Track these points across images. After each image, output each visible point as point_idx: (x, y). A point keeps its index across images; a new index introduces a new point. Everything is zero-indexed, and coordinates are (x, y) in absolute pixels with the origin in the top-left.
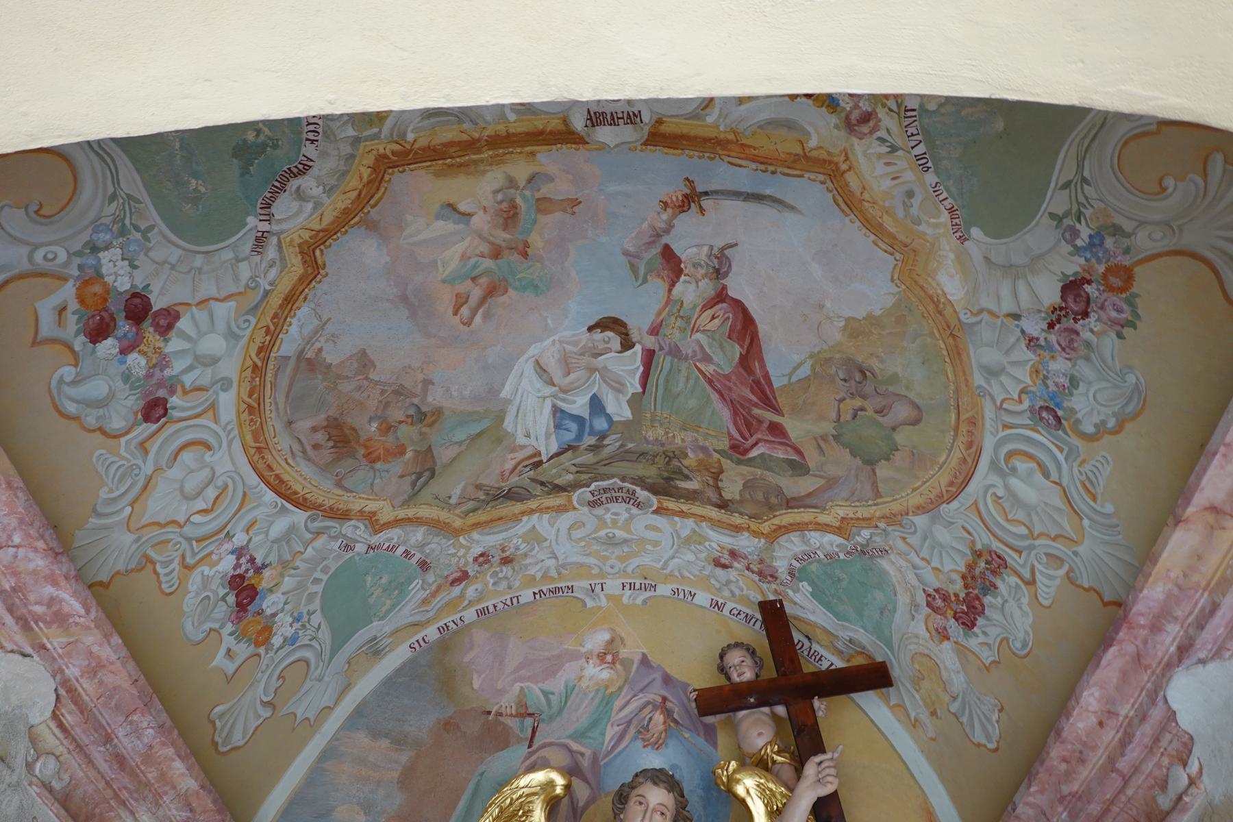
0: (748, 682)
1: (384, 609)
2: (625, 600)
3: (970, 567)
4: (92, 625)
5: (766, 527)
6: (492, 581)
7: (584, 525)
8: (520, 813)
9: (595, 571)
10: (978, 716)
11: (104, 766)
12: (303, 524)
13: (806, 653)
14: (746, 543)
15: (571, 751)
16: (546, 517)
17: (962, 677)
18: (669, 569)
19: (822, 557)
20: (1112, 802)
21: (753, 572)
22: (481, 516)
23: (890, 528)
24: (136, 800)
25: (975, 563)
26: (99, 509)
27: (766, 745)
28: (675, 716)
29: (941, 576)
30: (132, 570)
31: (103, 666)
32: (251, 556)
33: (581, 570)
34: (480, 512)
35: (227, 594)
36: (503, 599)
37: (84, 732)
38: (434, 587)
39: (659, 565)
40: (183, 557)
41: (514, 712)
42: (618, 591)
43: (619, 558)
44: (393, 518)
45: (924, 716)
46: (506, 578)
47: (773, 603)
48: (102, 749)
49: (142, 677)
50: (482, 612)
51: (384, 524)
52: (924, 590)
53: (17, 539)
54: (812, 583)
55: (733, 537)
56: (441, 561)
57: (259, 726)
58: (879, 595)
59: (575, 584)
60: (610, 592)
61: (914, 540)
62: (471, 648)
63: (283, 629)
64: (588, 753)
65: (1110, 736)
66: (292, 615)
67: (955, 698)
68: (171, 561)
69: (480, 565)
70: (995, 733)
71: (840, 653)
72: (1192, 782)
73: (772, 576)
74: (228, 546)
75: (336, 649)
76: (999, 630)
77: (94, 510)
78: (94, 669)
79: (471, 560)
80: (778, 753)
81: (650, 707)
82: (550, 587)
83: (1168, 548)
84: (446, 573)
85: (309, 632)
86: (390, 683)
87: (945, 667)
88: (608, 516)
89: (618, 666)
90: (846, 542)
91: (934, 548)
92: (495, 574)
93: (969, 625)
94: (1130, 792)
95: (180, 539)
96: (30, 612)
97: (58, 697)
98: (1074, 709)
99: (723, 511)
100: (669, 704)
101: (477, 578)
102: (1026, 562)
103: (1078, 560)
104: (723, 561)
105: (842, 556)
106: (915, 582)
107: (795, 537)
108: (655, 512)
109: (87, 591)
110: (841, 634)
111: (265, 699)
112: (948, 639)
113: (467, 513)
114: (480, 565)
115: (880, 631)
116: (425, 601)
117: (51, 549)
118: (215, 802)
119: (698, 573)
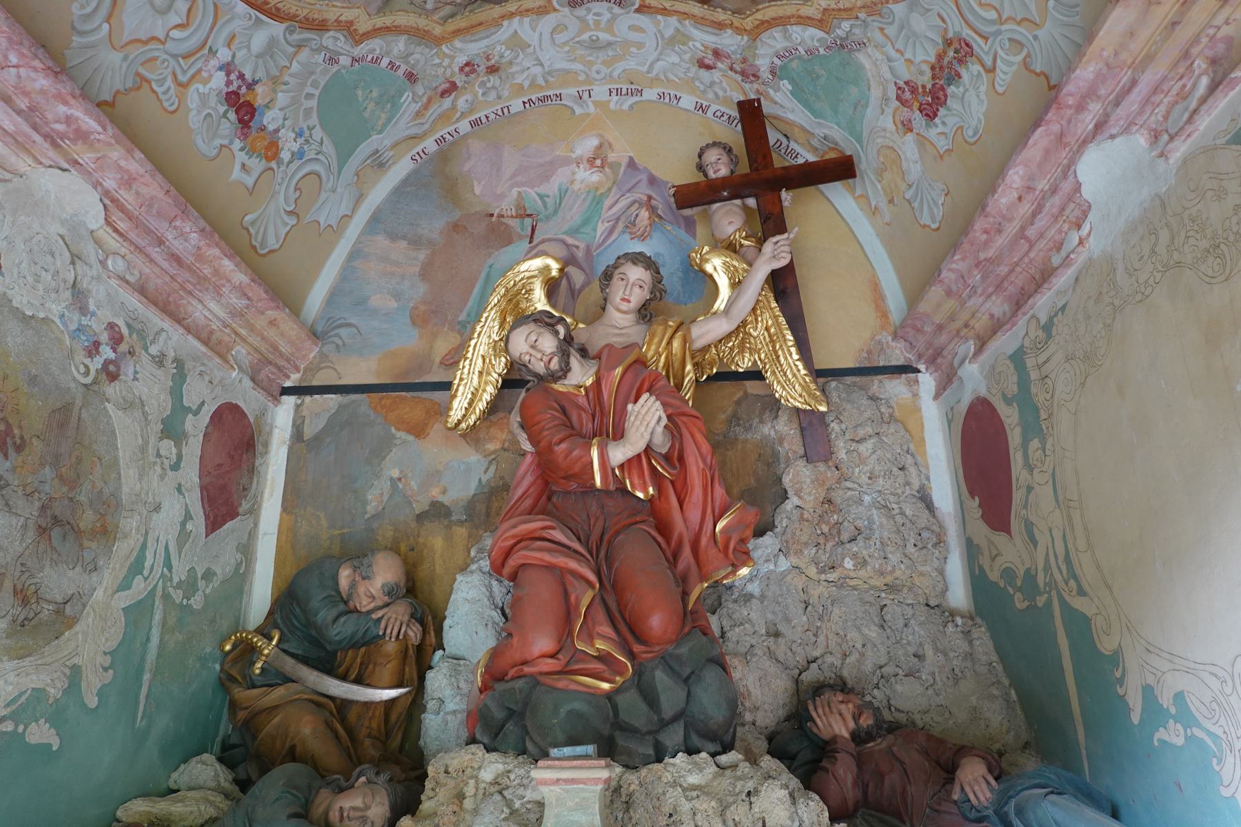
0: (724, 178)
1: (380, 123)
2: (612, 106)
3: (940, 57)
4: (113, 142)
5: (749, 23)
6: (481, 92)
7: (566, 27)
8: (523, 292)
9: (582, 77)
10: (928, 201)
11: (165, 265)
12: (282, 37)
13: (783, 151)
14: (730, 41)
15: (567, 245)
16: (526, 20)
17: (919, 167)
18: (655, 72)
19: (803, 53)
20: (1017, 264)
21: (736, 72)
22: (460, 22)
23: (870, 19)
24: (200, 291)
25: (945, 52)
26: (78, 26)
27: (736, 231)
28: (660, 212)
29: (912, 68)
30: (131, 89)
31: (135, 179)
32: (239, 72)
33: (568, 77)
34: (458, 17)
35: (226, 112)
36: (494, 109)
37: (138, 236)
38: (425, 99)
39: (645, 68)
40: (174, 74)
41: (514, 214)
42: (606, 97)
43: (604, 63)
44: (370, 28)
45: (883, 205)
46: (494, 87)
47: (751, 102)
48: (158, 249)
49: (172, 188)
50: (476, 123)
51: (364, 34)
52: (895, 83)
53: (14, 59)
54: (792, 81)
55: (716, 35)
56: (428, 72)
57: (288, 233)
58: (854, 90)
59: (563, 92)
60: (597, 98)
61: (891, 31)
62: (469, 158)
63: (288, 144)
64: (582, 245)
65: (1026, 208)
66: (293, 130)
67: (910, 186)
68: (164, 79)
69: (467, 75)
70: (939, 213)
71: (814, 150)
72: (1081, 242)
73: (754, 75)
74: (214, 63)
75: (343, 159)
76: (957, 119)
77: (73, 28)
78: (128, 181)
79: (457, 70)
80: (746, 238)
81: (637, 205)
82: (539, 95)
83: (1106, 27)
84: (434, 85)
85: (313, 147)
86: (399, 192)
87: (906, 158)
88: (590, 17)
89: (607, 169)
90: (826, 36)
91: (909, 38)
92: (483, 84)
93: (931, 115)
94: (1032, 255)
95: (166, 56)
96: (52, 129)
97: (105, 207)
98: (999, 186)
99: (706, 7)
100: (653, 202)
101: (465, 88)
102: (990, 49)
103: (1036, 44)
104: (707, 61)
105: (822, 51)
106: (888, 75)
107: (777, 33)
108: (638, 11)
109: (97, 109)
110: (817, 131)
111: (289, 209)
112: (912, 131)
113: (445, 20)
114: (467, 75)
115: (853, 128)
116: (418, 114)
117: (49, 68)
118: (266, 292)
119: (682, 76)
